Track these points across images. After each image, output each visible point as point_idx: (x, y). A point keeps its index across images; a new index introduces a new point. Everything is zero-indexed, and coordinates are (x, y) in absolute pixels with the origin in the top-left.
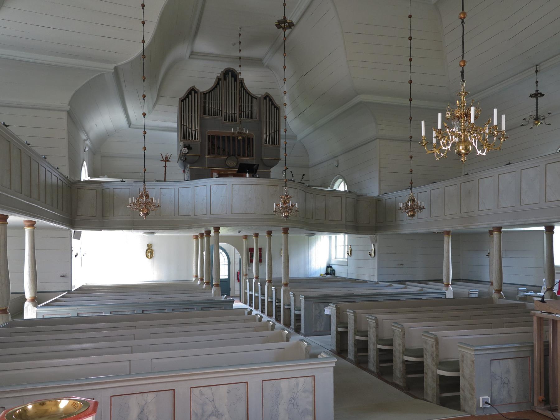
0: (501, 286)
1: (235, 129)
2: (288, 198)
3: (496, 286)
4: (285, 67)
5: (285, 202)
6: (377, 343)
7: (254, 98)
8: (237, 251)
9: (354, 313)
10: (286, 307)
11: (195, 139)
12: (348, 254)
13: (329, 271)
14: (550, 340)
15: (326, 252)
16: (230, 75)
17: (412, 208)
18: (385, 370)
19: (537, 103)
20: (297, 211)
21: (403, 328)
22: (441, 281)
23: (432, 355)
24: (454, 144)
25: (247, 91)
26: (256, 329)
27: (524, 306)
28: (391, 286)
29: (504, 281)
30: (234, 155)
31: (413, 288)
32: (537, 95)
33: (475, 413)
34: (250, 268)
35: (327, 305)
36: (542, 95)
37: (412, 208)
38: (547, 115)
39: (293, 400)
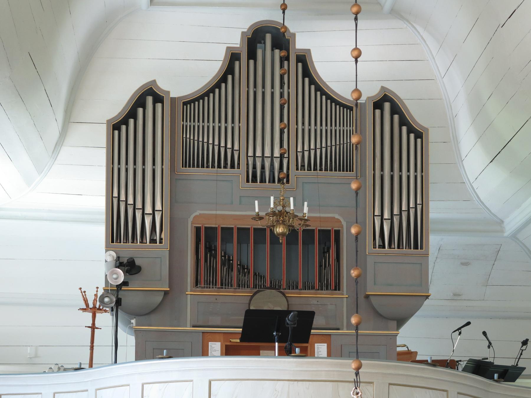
1: (264, 203)
11: (153, 241)
16: (268, 40)
25: (320, 89)
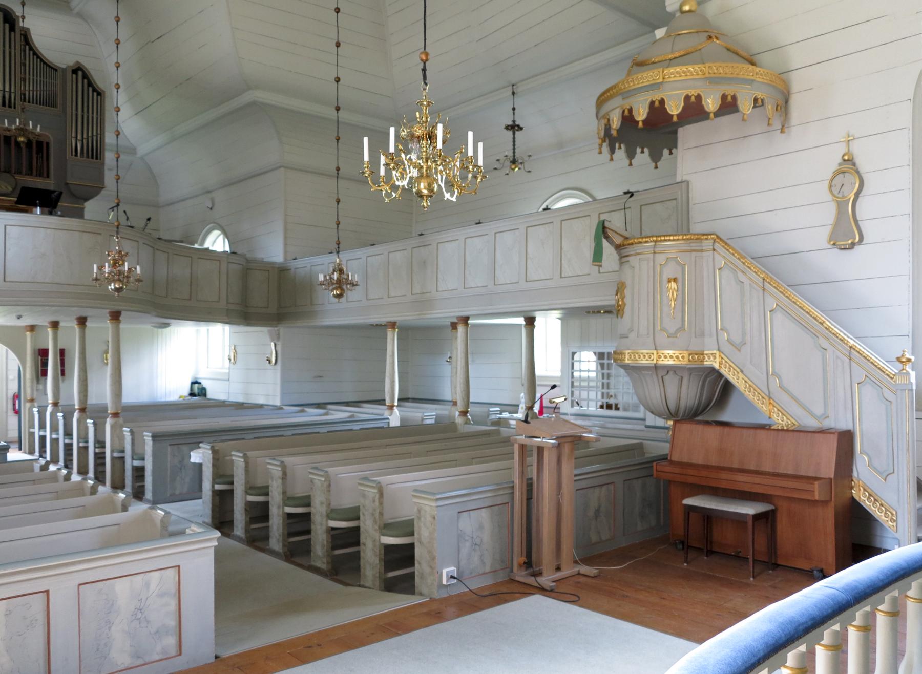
0: (467, 405)
2: (122, 256)
3: (460, 407)
4: (118, 20)
5: (115, 264)
6: (285, 505)
7: (55, 69)
8: (12, 355)
9: (245, 457)
10: (116, 455)
12: (230, 359)
13: (196, 391)
14: (535, 478)
15: (191, 358)
17: (339, 284)
18: (297, 550)
19: (514, 138)
20: (139, 280)
21: (327, 476)
22: (381, 402)
23: (373, 515)
24: (411, 178)
25: (36, 54)
26: (58, 495)
27: (498, 432)
28: (302, 411)
29: (471, 400)
30: (9, 172)
31: (339, 414)
32: (514, 127)
33: (437, 595)
34: (41, 387)
35: (196, 445)
36: (521, 128)
37: (339, 284)
38: (526, 158)
39: (139, 614)
